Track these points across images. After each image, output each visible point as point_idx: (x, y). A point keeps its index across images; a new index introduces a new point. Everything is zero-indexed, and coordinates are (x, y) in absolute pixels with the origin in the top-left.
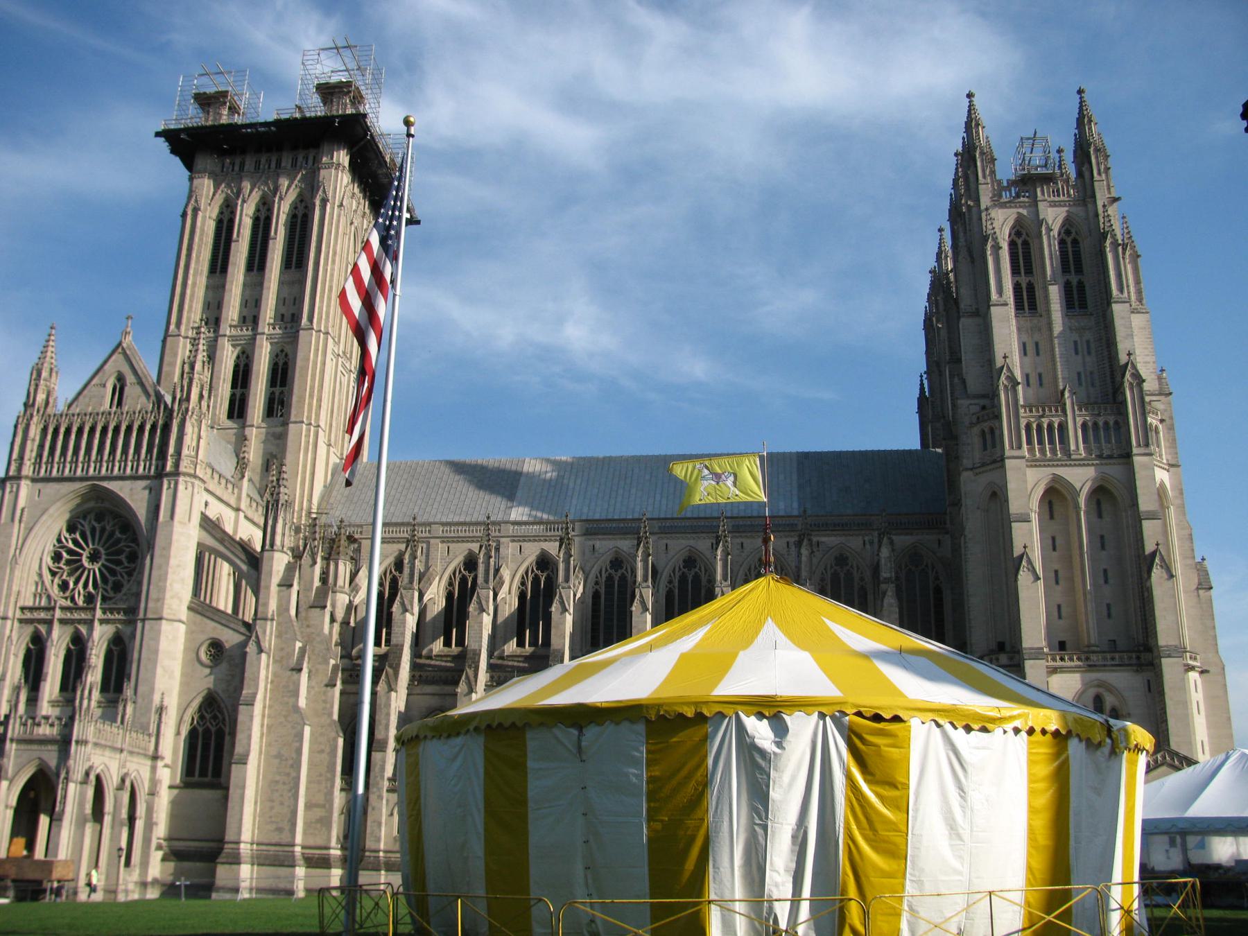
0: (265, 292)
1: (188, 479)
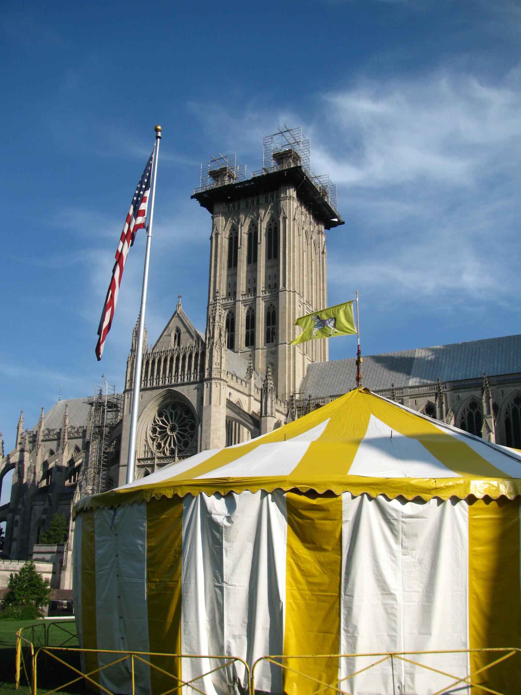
0: (258, 273)
1: (217, 381)
